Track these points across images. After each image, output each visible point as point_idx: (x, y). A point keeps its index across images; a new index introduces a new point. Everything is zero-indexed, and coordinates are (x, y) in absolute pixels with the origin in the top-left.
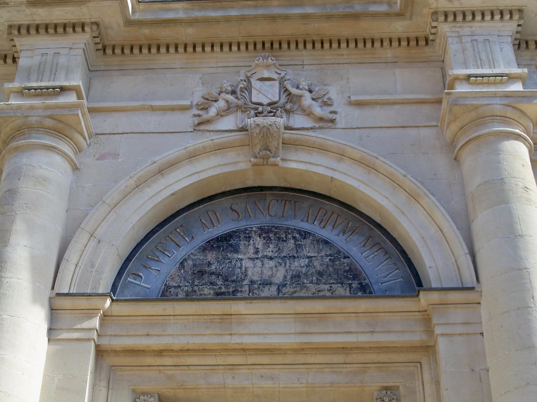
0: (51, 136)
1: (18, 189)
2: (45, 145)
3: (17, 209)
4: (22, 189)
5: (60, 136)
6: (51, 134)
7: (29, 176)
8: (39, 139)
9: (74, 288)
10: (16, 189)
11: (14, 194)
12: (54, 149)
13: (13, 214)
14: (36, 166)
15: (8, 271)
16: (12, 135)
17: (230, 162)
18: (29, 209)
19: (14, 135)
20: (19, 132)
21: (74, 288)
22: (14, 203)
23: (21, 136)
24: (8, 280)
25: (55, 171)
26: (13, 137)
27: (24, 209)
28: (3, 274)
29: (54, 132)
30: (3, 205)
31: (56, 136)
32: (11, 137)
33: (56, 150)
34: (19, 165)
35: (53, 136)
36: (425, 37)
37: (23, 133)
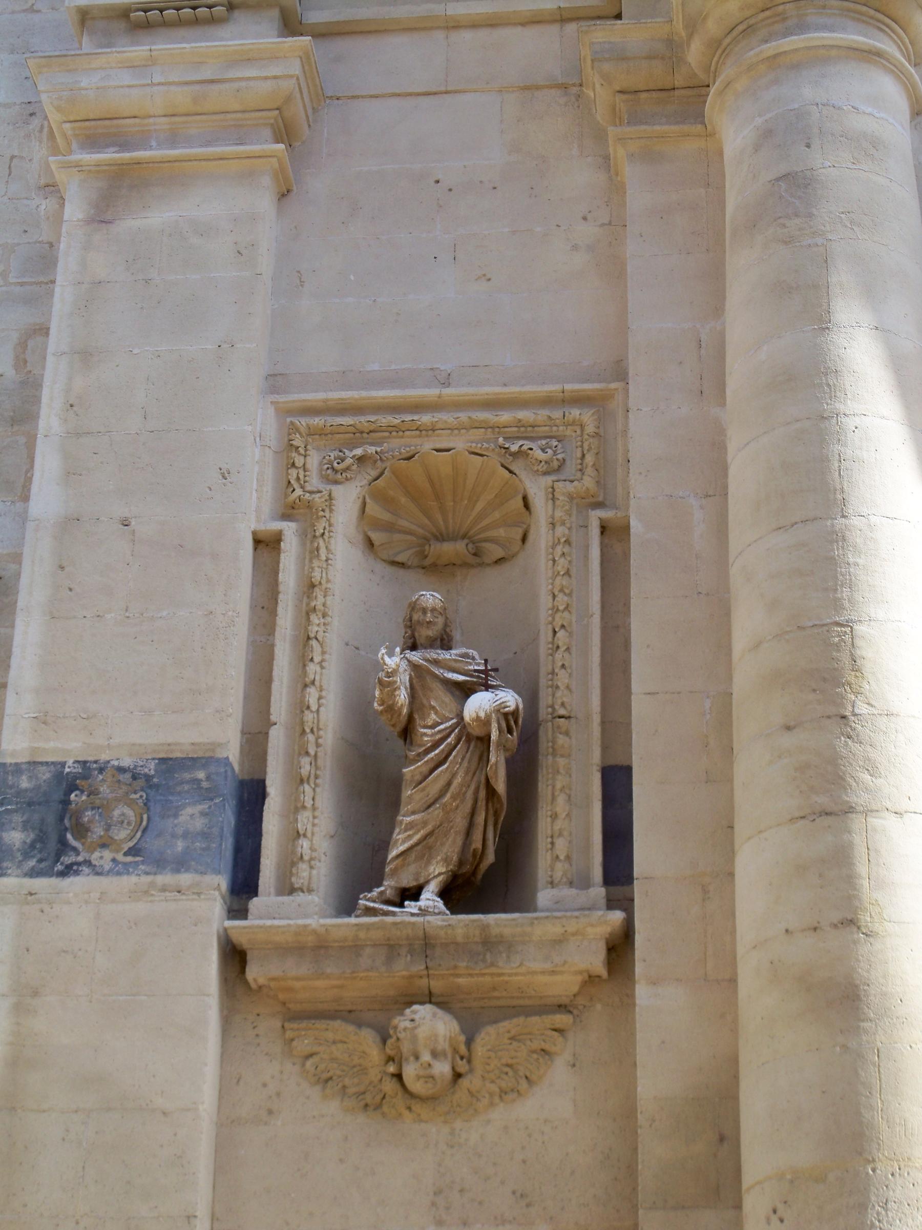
0: (858, 20)
1: (815, 173)
2: (855, 46)
3: (828, 228)
4: (823, 170)
5: (879, 21)
6: (857, 16)
7: (832, 134)
8: (831, 29)
9: (129, 52)
10: (808, 173)
11: (806, 186)
12: (878, 59)
13: (820, 241)
14: (845, 108)
15: (849, 396)
16: (746, 22)
17: (176, 80)
18: (859, 225)
19: (752, 21)
20: (768, 13)
21: (129, 52)
22: (814, 211)
23: (774, 23)
24: (857, 421)
25: (891, 121)
26: (749, 27)
27: (846, 226)
28: (841, 407)
29: (865, 9)
30: (780, 218)
31: (871, 21)
32: (741, 28)
33: (882, 61)
34: (796, 106)
35: (863, 22)
36: (35, 113)
37: (779, 15)
